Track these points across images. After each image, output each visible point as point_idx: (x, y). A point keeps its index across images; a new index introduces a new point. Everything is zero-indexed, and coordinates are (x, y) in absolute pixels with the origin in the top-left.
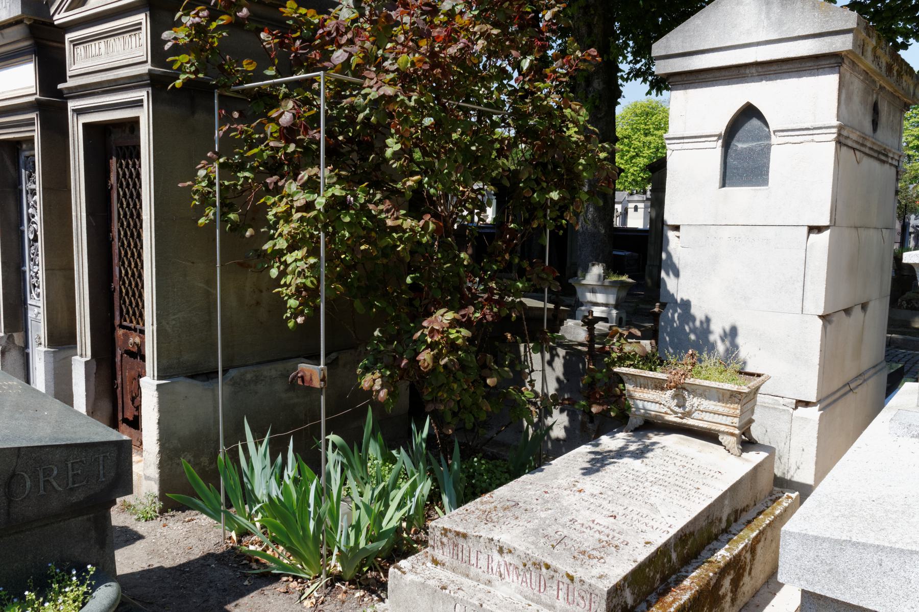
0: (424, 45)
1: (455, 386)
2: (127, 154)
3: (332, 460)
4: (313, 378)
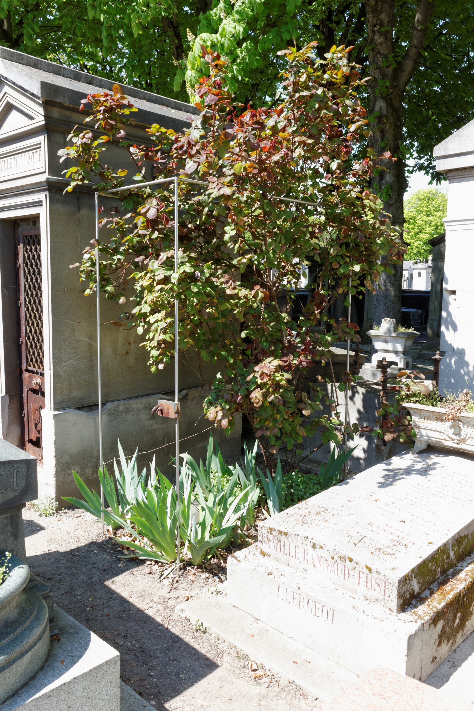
0: (254, 155)
1: (278, 417)
2: (31, 241)
4: (170, 411)
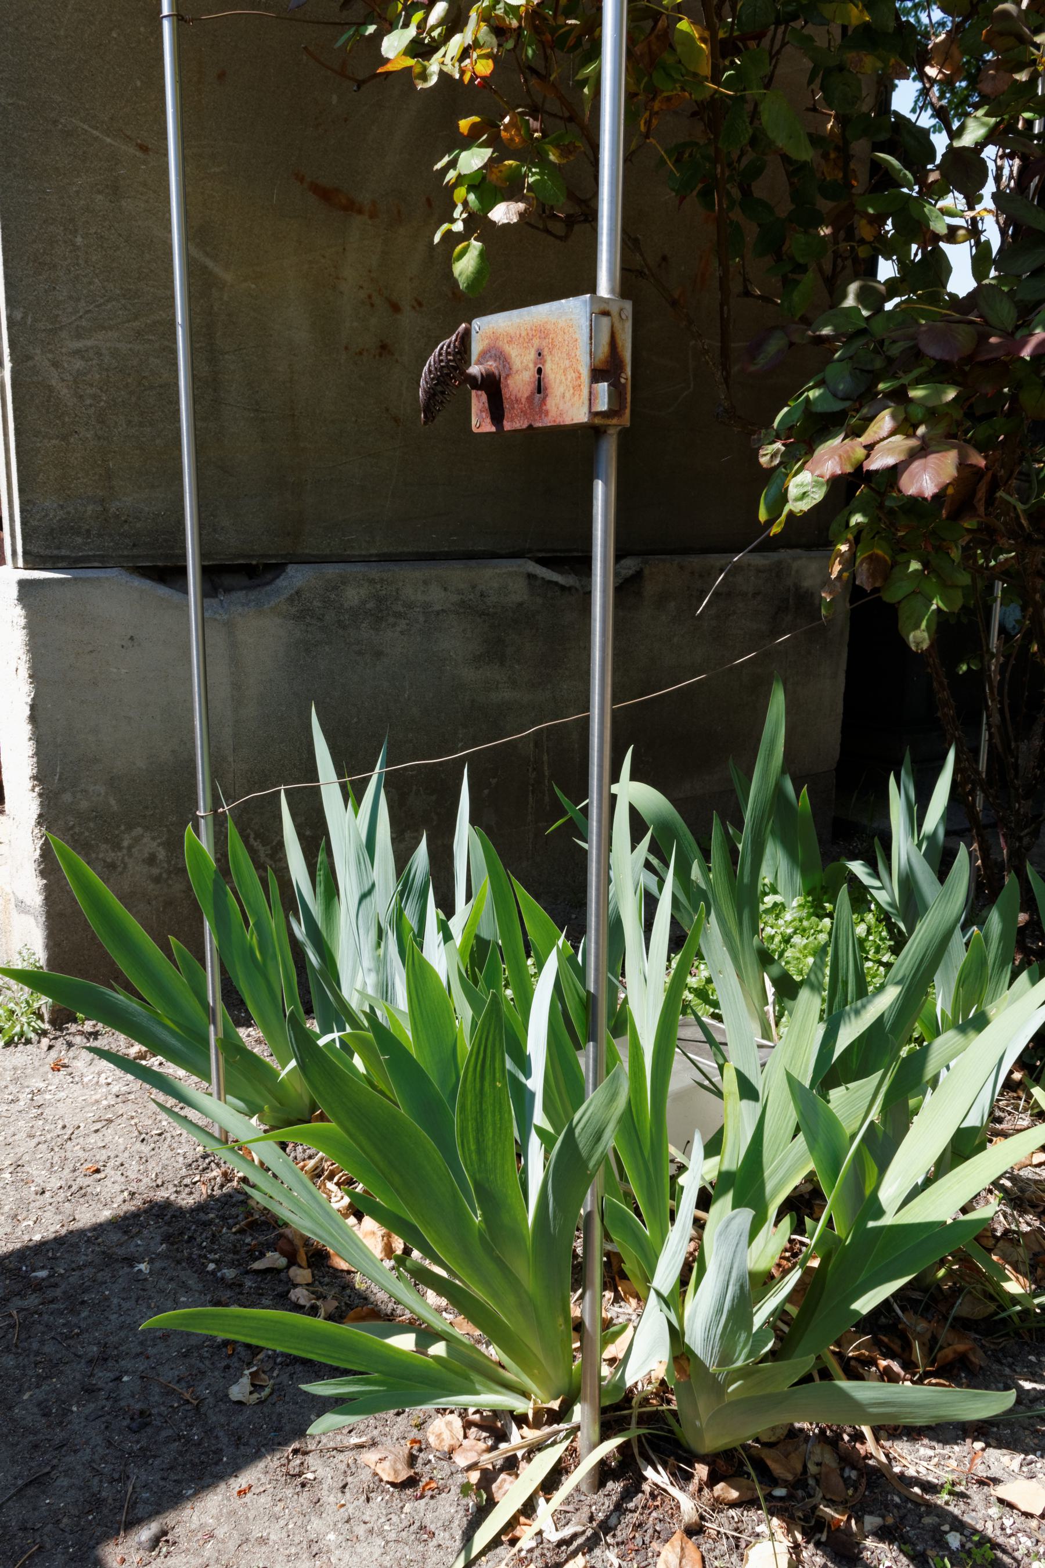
3: (623, 871)
